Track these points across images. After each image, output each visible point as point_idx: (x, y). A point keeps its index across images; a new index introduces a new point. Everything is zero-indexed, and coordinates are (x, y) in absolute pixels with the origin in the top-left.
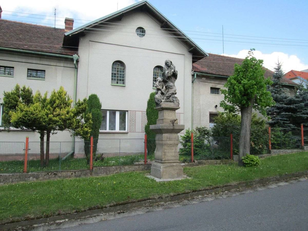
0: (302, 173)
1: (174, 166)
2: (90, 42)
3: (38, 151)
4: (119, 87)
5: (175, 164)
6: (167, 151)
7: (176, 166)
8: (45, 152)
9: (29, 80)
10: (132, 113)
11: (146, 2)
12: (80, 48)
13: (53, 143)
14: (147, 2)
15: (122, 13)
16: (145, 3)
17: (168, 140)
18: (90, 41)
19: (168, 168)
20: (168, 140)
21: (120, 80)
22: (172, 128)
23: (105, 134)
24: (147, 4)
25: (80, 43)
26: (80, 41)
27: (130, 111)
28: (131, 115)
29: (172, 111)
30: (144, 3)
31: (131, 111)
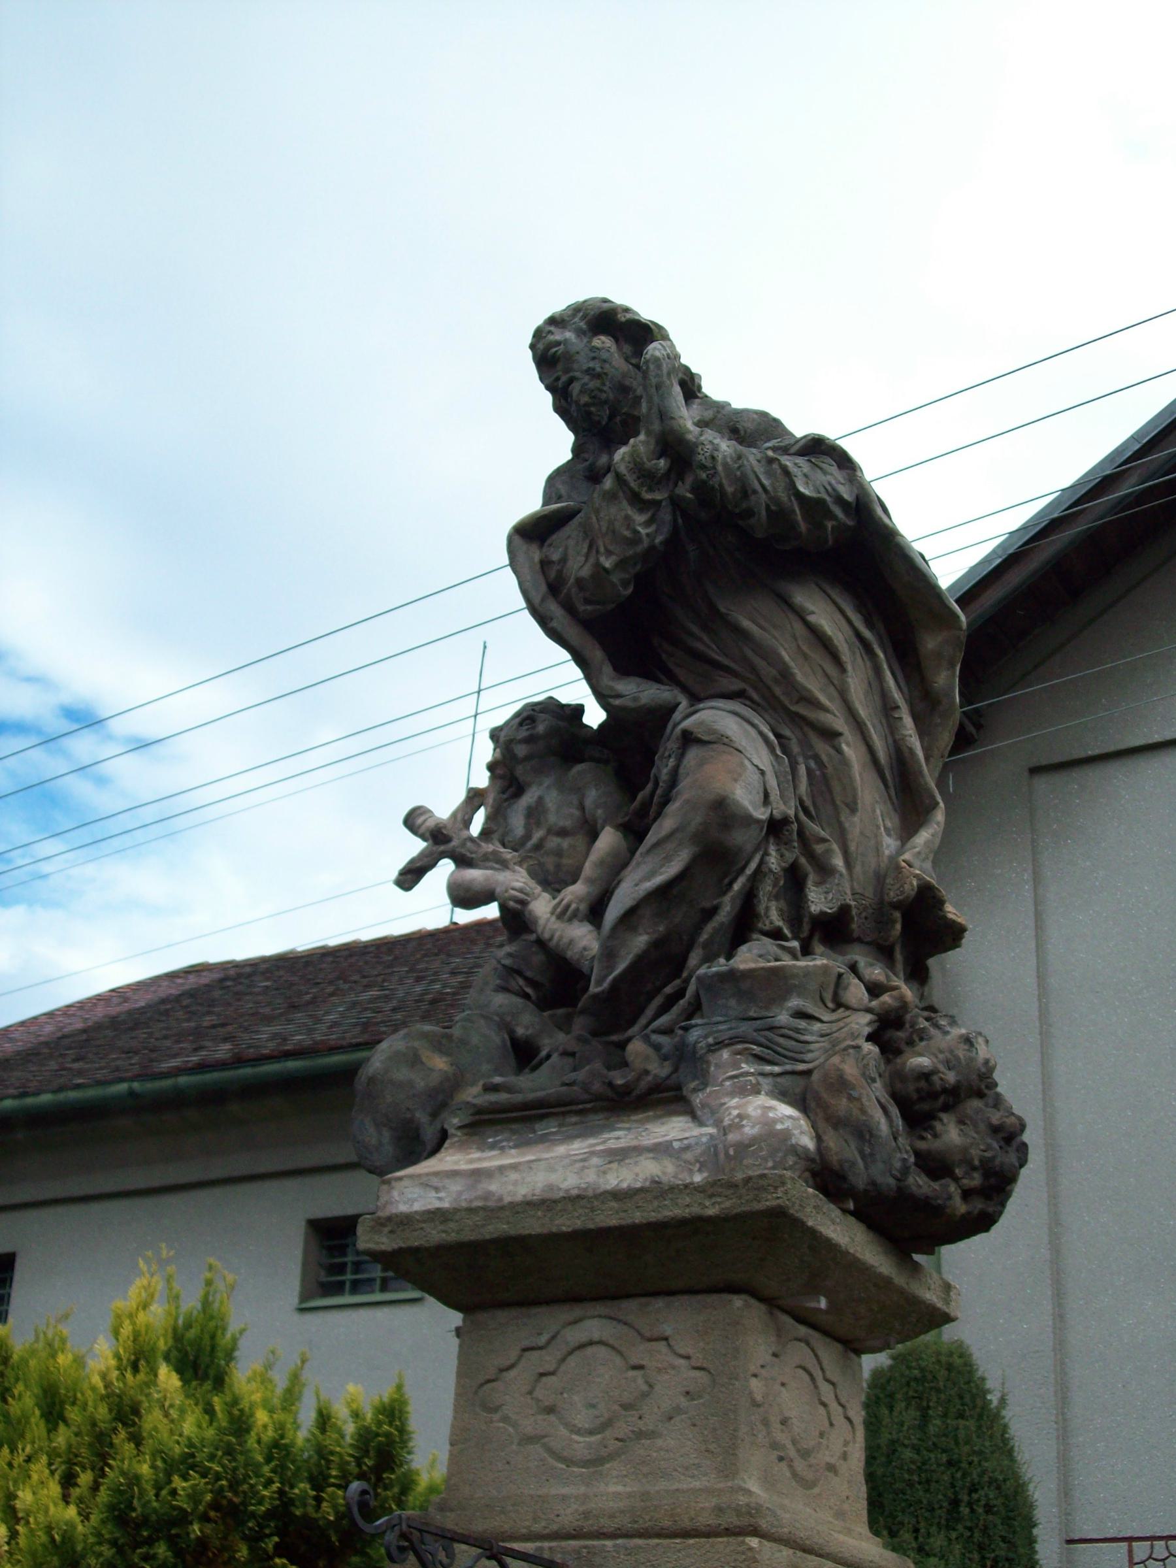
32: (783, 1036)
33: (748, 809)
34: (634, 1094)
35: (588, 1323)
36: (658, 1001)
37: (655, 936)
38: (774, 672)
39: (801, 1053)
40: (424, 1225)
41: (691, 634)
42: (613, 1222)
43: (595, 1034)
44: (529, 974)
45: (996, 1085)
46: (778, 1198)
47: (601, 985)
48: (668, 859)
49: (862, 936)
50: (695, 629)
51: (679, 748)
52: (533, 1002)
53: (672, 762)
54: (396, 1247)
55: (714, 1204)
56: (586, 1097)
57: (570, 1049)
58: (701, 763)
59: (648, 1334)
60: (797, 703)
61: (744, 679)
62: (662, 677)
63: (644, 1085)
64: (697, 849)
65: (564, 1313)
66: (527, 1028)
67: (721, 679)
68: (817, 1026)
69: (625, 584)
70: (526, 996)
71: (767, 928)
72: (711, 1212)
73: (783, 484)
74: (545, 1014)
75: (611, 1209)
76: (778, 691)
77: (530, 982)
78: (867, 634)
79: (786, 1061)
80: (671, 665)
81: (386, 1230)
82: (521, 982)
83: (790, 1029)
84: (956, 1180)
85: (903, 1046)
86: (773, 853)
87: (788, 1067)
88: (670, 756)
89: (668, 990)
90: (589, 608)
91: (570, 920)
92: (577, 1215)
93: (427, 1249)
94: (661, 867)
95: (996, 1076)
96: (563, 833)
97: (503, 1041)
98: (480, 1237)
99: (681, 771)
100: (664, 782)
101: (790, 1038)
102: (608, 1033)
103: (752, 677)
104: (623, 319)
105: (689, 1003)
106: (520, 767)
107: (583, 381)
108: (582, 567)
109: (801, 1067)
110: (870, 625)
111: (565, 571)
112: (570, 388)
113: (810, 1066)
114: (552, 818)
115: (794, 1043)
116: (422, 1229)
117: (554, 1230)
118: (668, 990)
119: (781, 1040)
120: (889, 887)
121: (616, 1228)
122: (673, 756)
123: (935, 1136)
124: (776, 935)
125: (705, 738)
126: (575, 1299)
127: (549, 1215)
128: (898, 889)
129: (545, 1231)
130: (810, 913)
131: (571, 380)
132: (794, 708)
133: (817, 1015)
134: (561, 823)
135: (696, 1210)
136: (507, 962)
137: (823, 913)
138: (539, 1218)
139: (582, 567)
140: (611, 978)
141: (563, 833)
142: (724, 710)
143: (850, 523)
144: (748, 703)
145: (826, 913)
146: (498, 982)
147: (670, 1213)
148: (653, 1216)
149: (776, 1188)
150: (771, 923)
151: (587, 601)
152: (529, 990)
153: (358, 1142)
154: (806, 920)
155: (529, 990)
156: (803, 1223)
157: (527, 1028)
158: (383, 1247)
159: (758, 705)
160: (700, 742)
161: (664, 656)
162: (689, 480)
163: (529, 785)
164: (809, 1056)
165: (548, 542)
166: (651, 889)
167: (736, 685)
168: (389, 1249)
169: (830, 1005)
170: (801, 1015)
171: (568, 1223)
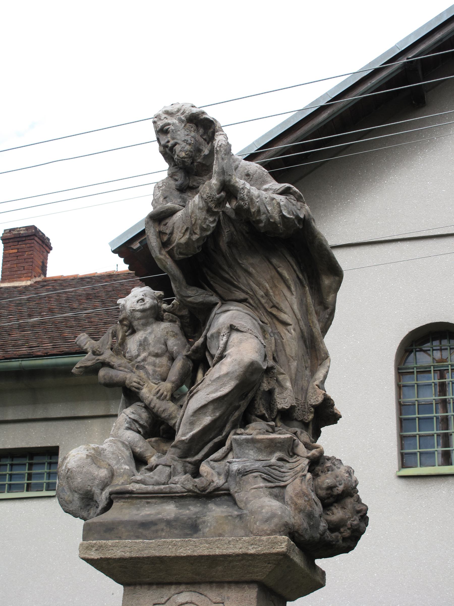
32: (273, 469)
33: (261, 366)
34: (207, 491)
35: (184, 594)
36: (210, 445)
37: (214, 417)
38: (262, 293)
39: (282, 477)
40: (114, 548)
41: (224, 270)
42: (206, 553)
43: (272, 510)
44: (141, 422)
45: (358, 491)
46: (283, 548)
47: (185, 436)
48: (224, 385)
49: (297, 418)
50: (226, 268)
51: (228, 333)
52: (142, 435)
53: (225, 339)
54: (99, 557)
55: (253, 548)
56: (184, 490)
57: (168, 463)
58: (240, 342)
59: (214, 601)
60: (271, 308)
61: (247, 293)
62: (207, 288)
63: (210, 489)
64: (238, 382)
65: (173, 589)
66: (140, 448)
67: (236, 292)
68: (288, 465)
69: (198, 248)
70: (139, 432)
71: (259, 414)
72: (252, 551)
73: (277, 211)
74: (147, 440)
75: (205, 547)
76: (263, 301)
77: (141, 426)
78: (301, 276)
79: (277, 481)
80: (212, 283)
81: (94, 549)
82: (137, 426)
83: (277, 466)
84: (341, 533)
85: (320, 473)
86: (265, 382)
87: (277, 484)
88: (224, 335)
89: (216, 440)
90: (181, 256)
91: (163, 400)
92: (188, 548)
93: (114, 559)
94: (220, 388)
95: (358, 487)
96: (157, 355)
97: (130, 453)
98: (141, 556)
99: (229, 343)
100: (221, 348)
101: (277, 470)
102: (186, 457)
103: (251, 293)
104: (202, 117)
105: (228, 449)
106: (136, 322)
107: (182, 146)
108: (181, 238)
109: (282, 484)
110: (302, 272)
111: (172, 238)
112: (174, 148)
113: (286, 483)
114: (152, 349)
115: (279, 472)
116: (112, 550)
117: (178, 555)
118: (216, 440)
119: (273, 471)
120: (310, 397)
121: (207, 556)
122: (225, 336)
123: (333, 514)
124: (263, 418)
125: (242, 329)
126: (178, 583)
127: (175, 548)
128: (315, 399)
129: (173, 555)
130: (277, 408)
131: (176, 144)
132: (269, 310)
133: (287, 459)
134: (156, 351)
135: (244, 550)
136: (132, 416)
137: (283, 408)
138: (170, 549)
139: (181, 238)
140: (191, 434)
141: (157, 355)
142: (243, 312)
143: (301, 227)
144: (248, 304)
145: (284, 408)
146: (127, 425)
147: (233, 551)
148: (225, 552)
149: (281, 543)
150: (261, 412)
151: (181, 253)
152: (140, 429)
153: (61, 498)
154: (275, 410)
155: (140, 429)
156: (289, 557)
157: (140, 448)
158: (92, 557)
159: (253, 306)
160: (238, 330)
161: (209, 278)
162: (234, 203)
163: (139, 330)
164: (285, 479)
165: (164, 223)
166: (216, 398)
167: (242, 296)
168: (96, 558)
169: (291, 454)
170: (280, 459)
171: (184, 552)
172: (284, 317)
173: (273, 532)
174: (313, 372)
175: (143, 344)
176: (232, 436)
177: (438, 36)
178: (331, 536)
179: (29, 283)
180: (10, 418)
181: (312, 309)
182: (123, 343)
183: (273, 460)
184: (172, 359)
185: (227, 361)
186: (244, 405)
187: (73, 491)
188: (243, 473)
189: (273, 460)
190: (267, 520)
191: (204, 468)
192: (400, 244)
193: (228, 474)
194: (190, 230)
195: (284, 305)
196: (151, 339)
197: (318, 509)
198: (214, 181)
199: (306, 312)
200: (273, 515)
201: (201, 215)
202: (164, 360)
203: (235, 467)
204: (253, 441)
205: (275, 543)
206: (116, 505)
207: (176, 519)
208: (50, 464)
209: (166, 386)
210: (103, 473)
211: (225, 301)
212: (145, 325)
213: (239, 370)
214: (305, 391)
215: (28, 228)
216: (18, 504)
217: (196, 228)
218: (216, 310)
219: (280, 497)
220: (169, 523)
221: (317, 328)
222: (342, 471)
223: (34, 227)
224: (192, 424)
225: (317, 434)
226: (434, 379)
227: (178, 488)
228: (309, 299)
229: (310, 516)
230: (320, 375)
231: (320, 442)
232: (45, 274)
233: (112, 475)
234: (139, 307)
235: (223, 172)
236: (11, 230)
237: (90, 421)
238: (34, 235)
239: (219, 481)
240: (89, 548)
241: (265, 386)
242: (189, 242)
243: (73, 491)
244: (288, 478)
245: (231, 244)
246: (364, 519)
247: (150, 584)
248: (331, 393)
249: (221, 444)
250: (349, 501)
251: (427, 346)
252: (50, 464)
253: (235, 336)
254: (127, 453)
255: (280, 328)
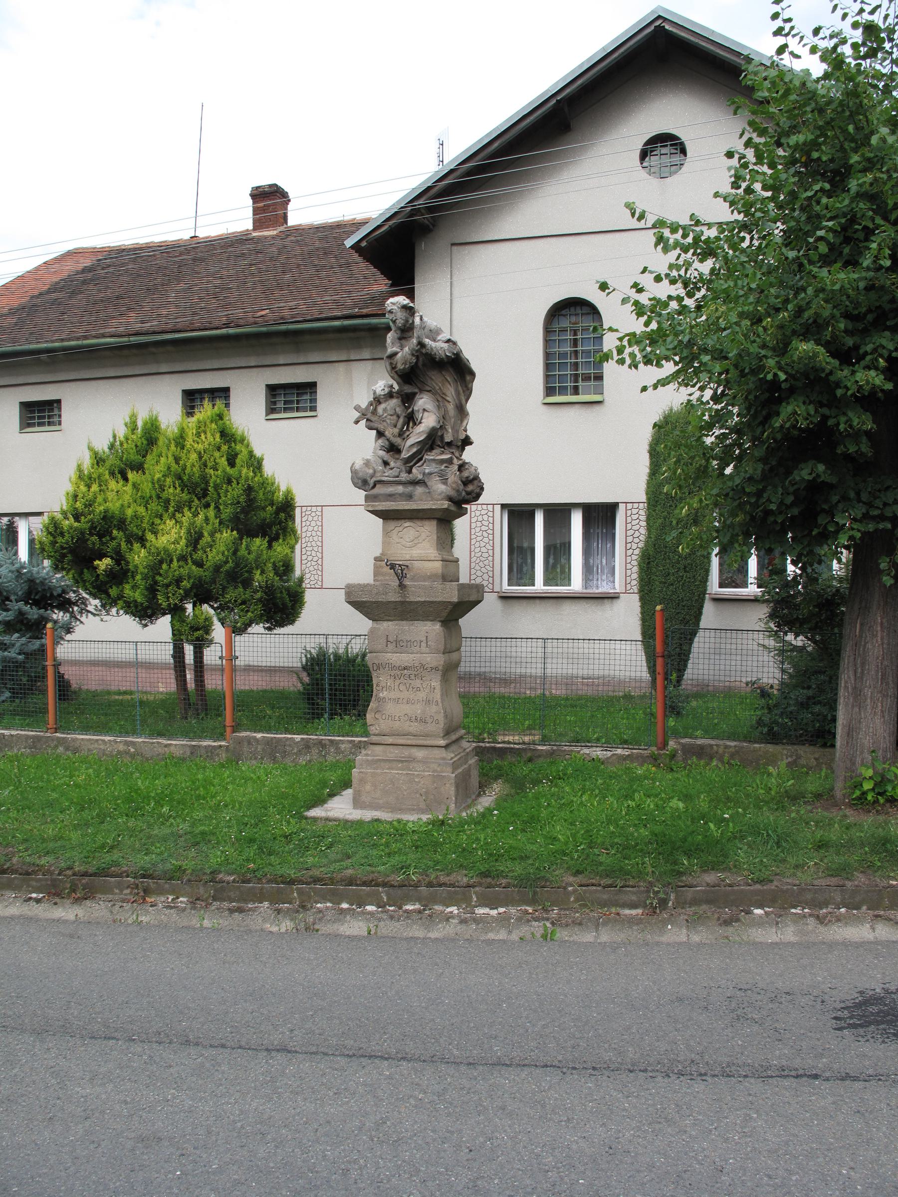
0: (433, 823)
1: (412, 760)
2: (455, 248)
3: (173, 687)
4: (577, 406)
5: (420, 754)
6: (393, 695)
7: (424, 761)
8: (191, 684)
9: (273, 423)
10: (635, 511)
11: (659, 17)
12: (417, 279)
13: (734, 634)
14: (665, 19)
15: (553, 102)
16: (657, 23)
17: (391, 647)
18: (453, 245)
19: (387, 765)
20: (391, 647)
21: (587, 378)
22: (393, 597)
23: (737, 604)
24: (667, 27)
25: (416, 261)
26: (416, 251)
27: (626, 503)
28: (629, 520)
29: (419, 523)
30: (652, 28)
31: (629, 506)
65: (403, 521)
124: (439, 446)
126: (405, 519)
167: (429, 389)
172: (448, 399)
173: (442, 499)
174: (462, 421)
175: (385, 410)
176: (426, 457)
177: (579, 82)
178: (467, 497)
179: (275, 233)
180: (281, 362)
181: (461, 392)
182: (375, 409)
183: (443, 467)
184: (398, 417)
185: (423, 425)
186: (430, 442)
187: (359, 479)
188: (430, 474)
189: (443, 467)
190: (440, 494)
191: (414, 470)
192: (549, 239)
193: (424, 474)
194: (405, 363)
195: (448, 393)
196: (388, 408)
197: (462, 487)
198: (415, 341)
199: (458, 394)
200: (442, 492)
201: (409, 357)
202: (395, 417)
203: (427, 471)
204: (434, 460)
205: (443, 504)
206: (377, 486)
207: (403, 493)
208: (311, 393)
209: (396, 431)
210: (371, 471)
211: (421, 391)
212: (385, 401)
213: (428, 430)
214: (457, 432)
215: (271, 186)
216: (292, 421)
217: (420, 819)
218: (417, 396)
219: (445, 483)
220: (400, 495)
221: (464, 401)
222: (472, 469)
223: (276, 185)
224: (408, 451)
225: (463, 449)
226: (569, 336)
227: (403, 479)
228: (460, 388)
229: (458, 491)
230: (464, 424)
231: (463, 457)
232: (286, 223)
233: (375, 472)
234: (382, 393)
235: (419, 337)
236: (257, 188)
237: (337, 364)
238: (276, 192)
239: (420, 477)
240: (368, 506)
241: (440, 434)
242: (404, 369)
243: (359, 479)
244: (449, 475)
245: (424, 365)
246: (482, 489)
247: (393, 519)
248: (469, 433)
249: (421, 459)
250: (476, 482)
251: (563, 312)
252: (311, 393)
253: (426, 414)
254: (380, 461)
255: (446, 403)
